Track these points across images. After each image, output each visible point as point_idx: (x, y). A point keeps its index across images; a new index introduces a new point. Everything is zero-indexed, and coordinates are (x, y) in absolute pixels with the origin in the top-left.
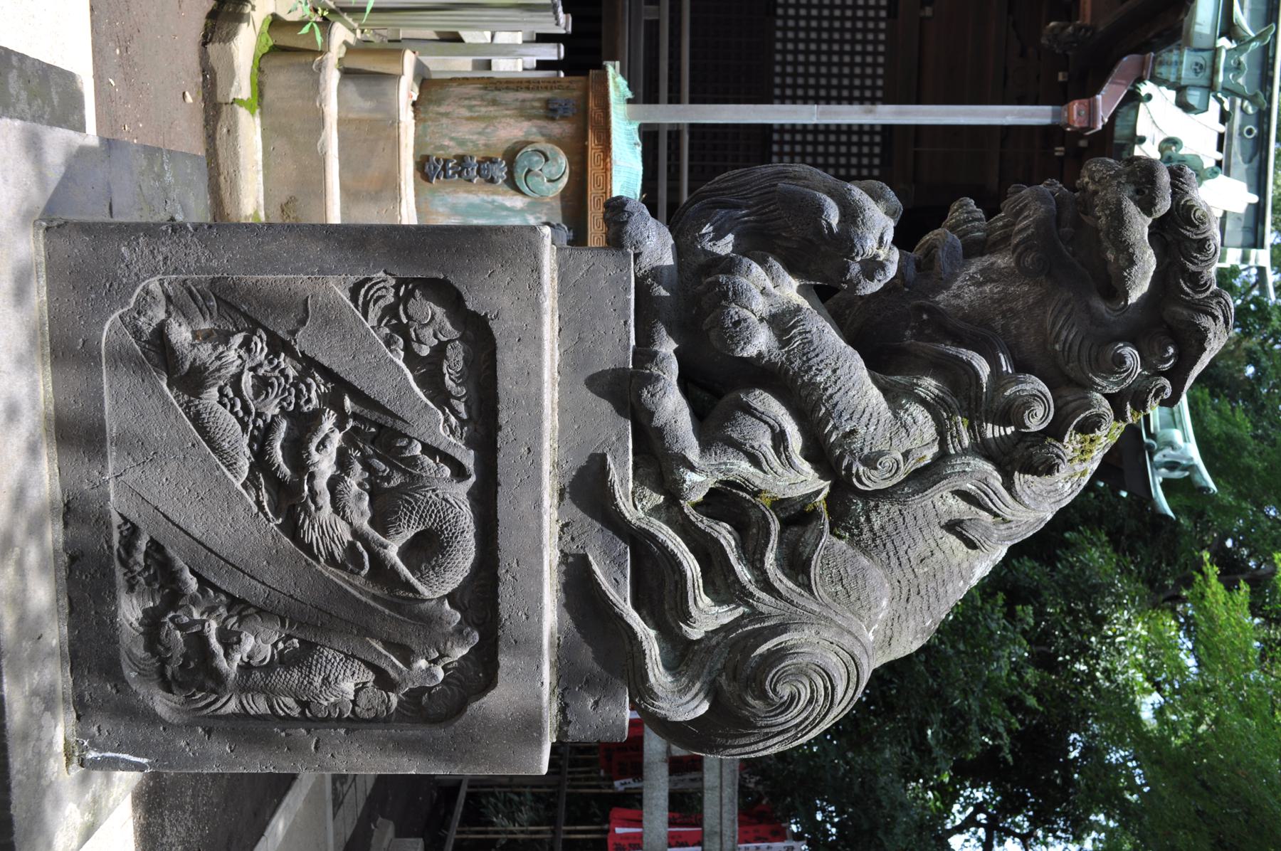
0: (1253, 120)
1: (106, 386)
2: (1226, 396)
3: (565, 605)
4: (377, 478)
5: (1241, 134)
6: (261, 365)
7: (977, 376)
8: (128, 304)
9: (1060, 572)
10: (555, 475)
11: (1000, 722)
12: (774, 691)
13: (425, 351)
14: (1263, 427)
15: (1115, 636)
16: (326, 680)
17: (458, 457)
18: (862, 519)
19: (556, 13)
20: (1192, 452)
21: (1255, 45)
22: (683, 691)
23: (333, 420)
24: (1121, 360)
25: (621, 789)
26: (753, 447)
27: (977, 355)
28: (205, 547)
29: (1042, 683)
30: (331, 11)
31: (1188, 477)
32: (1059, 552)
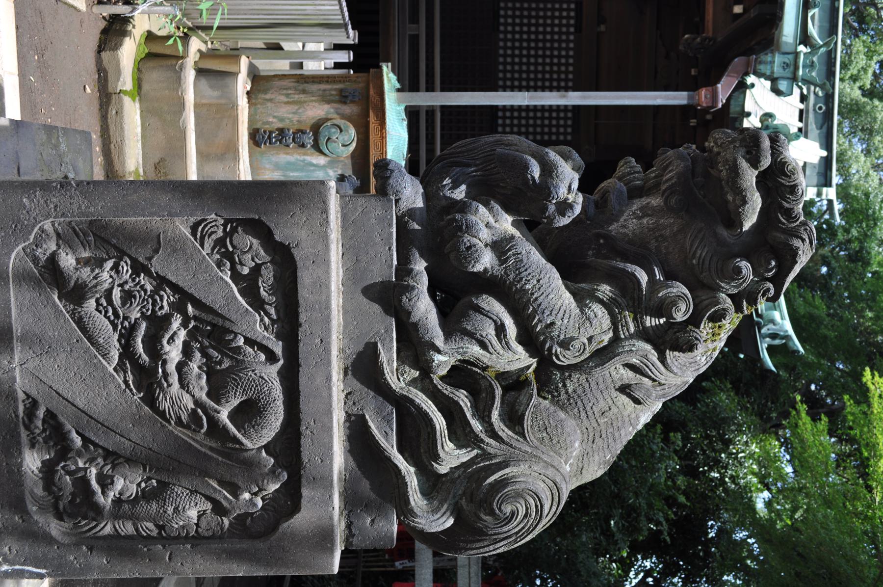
0: (823, 100)
1: (12, 299)
2: (808, 287)
3: (349, 451)
4: (212, 362)
5: (814, 110)
6: (126, 282)
7: (639, 283)
8: (29, 239)
9: (700, 409)
10: (341, 358)
11: (661, 514)
12: (500, 509)
13: (246, 271)
14: (834, 308)
15: (738, 453)
16: (176, 509)
17: (270, 346)
18: (560, 385)
19: (347, 29)
20: (787, 326)
21: (823, 50)
22: (434, 511)
23: (179, 321)
24: (739, 270)
25: (400, 567)
26: (481, 336)
27: (638, 269)
28: (87, 414)
29: (688, 486)
30: (190, 29)
31: (785, 343)
32: (698, 396)
